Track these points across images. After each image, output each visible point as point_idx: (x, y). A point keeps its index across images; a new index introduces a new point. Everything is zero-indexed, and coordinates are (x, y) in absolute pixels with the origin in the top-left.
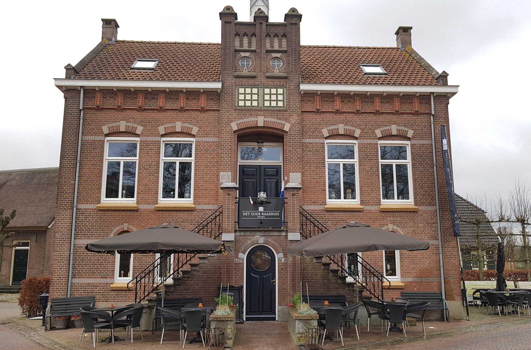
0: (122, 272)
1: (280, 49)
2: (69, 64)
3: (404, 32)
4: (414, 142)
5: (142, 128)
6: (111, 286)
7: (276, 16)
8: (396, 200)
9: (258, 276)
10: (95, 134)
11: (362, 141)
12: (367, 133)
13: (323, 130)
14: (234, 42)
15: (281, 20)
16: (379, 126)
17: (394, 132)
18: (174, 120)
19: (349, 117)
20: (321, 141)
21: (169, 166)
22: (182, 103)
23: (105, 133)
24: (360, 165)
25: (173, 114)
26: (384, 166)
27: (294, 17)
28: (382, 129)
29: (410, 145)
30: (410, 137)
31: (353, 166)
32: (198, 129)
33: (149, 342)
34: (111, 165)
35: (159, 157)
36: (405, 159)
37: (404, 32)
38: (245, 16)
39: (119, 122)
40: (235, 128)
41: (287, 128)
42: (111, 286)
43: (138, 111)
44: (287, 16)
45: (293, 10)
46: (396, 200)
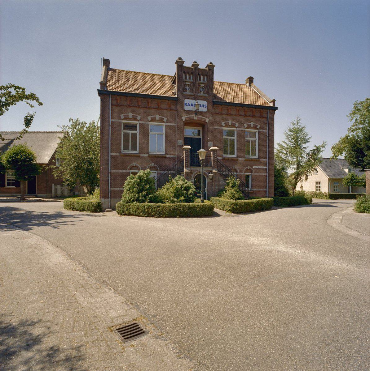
4: (238, 129)
8: (229, 155)
10: (219, 126)
11: (167, 124)
12: (241, 126)
13: (245, 124)
16: (246, 122)
19: (234, 117)
21: (126, 135)
23: (223, 126)
24: (237, 141)
26: (125, 134)
27: (211, 67)
29: (258, 132)
30: (237, 127)
31: (136, 134)
33: (304, 206)
34: (125, 134)
35: (230, 136)
39: (129, 113)
40: (184, 120)
41: (207, 121)
44: (208, 66)
46: (229, 155)
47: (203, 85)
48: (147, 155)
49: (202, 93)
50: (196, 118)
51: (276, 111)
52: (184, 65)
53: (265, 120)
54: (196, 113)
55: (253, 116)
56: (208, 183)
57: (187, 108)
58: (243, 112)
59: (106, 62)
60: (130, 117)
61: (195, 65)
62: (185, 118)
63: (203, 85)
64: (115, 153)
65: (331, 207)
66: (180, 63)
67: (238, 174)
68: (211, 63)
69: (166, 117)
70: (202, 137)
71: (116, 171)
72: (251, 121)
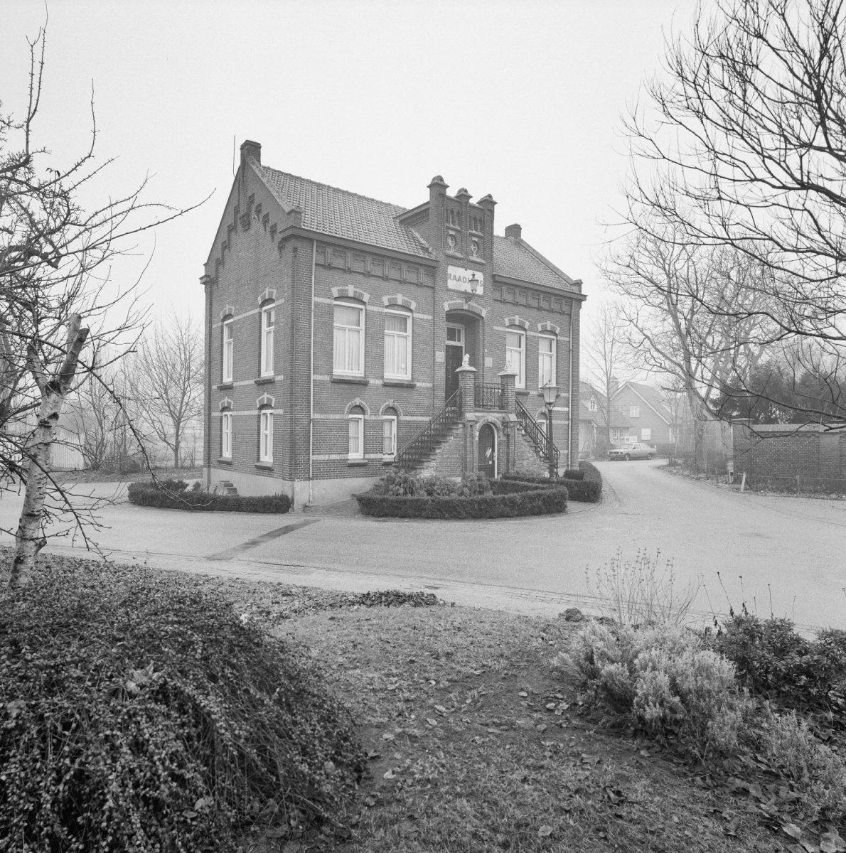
40: (447, 309)
41: (483, 315)
47: (476, 240)
48: (327, 378)
49: (474, 255)
50: (466, 307)
51: (583, 303)
52: (474, 201)
53: (566, 318)
54: (468, 297)
55: (551, 311)
56: (499, 444)
57: (451, 284)
58: (536, 301)
59: (251, 150)
60: (349, 295)
61: (464, 195)
62: (449, 305)
63: (476, 240)
64: (321, 374)
65: (211, 509)
66: (438, 186)
67: (367, 417)
68: (490, 196)
69: (414, 299)
70: (463, 346)
71: (323, 416)
72: (514, 315)
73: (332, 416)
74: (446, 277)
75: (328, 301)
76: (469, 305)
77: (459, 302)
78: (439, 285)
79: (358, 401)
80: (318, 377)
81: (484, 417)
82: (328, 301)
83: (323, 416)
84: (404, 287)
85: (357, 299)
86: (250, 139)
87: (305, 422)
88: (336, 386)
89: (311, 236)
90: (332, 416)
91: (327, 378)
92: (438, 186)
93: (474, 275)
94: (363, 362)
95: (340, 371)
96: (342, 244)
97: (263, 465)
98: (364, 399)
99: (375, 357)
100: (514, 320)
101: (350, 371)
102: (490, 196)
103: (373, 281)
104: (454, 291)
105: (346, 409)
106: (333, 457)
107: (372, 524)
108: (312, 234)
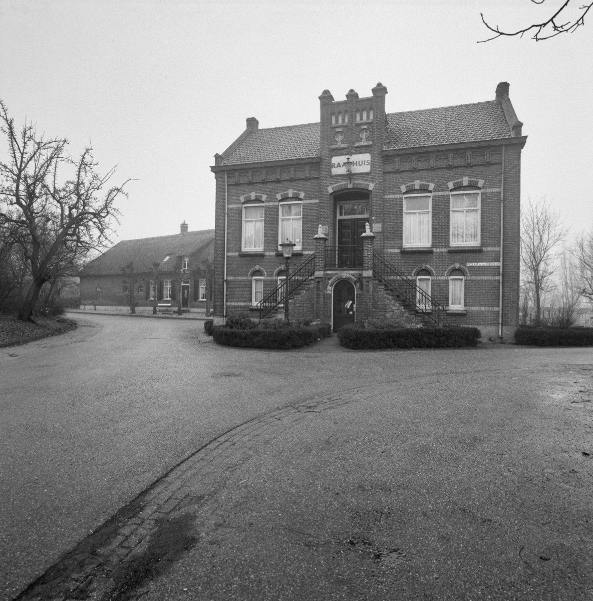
0: (159, 305)
1: (368, 121)
2: (217, 154)
3: (503, 89)
5: (484, 181)
6: (448, 312)
7: (365, 93)
9: (182, 309)
14: (356, 116)
15: (371, 95)
17: (417, 187)
18: (287, 189)
19: (425, 174)
20: (400, 196)
22: (292, 174)
25: (461, 170)
28: (281, 193)
29: (480, 194)
32: (484, 181)
36: (428, 209)
37: (503, 89)
38: (339, 96)
42: (448, 312)
43: (395, 173)
45: (379, 85)
48: (237, 254)
60: (416, 188)
71: (234, 278)
73: (240, 278)
74: (331, 166)
75: (238, 206)
76: (354, 184)
77: (342, 183)
78: (324, 173)
79: (257, 267)
80: (231, 254)
81: (336, 274)
82: (238, 206)
83: (234, 278)
84: (294, 183)
85: (258, 200)
86: (248, 117)
87: (221, 281)
88: (242, 258)
89: (500, 143)
90: (240, 278)
91: (397, 251)
92: (326, 98)
93: (348, 159)
94: (242, 244)
95: (246, 249)
96: (463, 147)
97: (451, 312)
98: (262, 266)
99: (441, 229)
100: (428, 186)
101: (465, 243)
102: (379, 85)
103: (269, 186)
104: (338, 176)
105: (414, 272)
106: (240, 304)
107: (357, 356)
108: (465, 144)
